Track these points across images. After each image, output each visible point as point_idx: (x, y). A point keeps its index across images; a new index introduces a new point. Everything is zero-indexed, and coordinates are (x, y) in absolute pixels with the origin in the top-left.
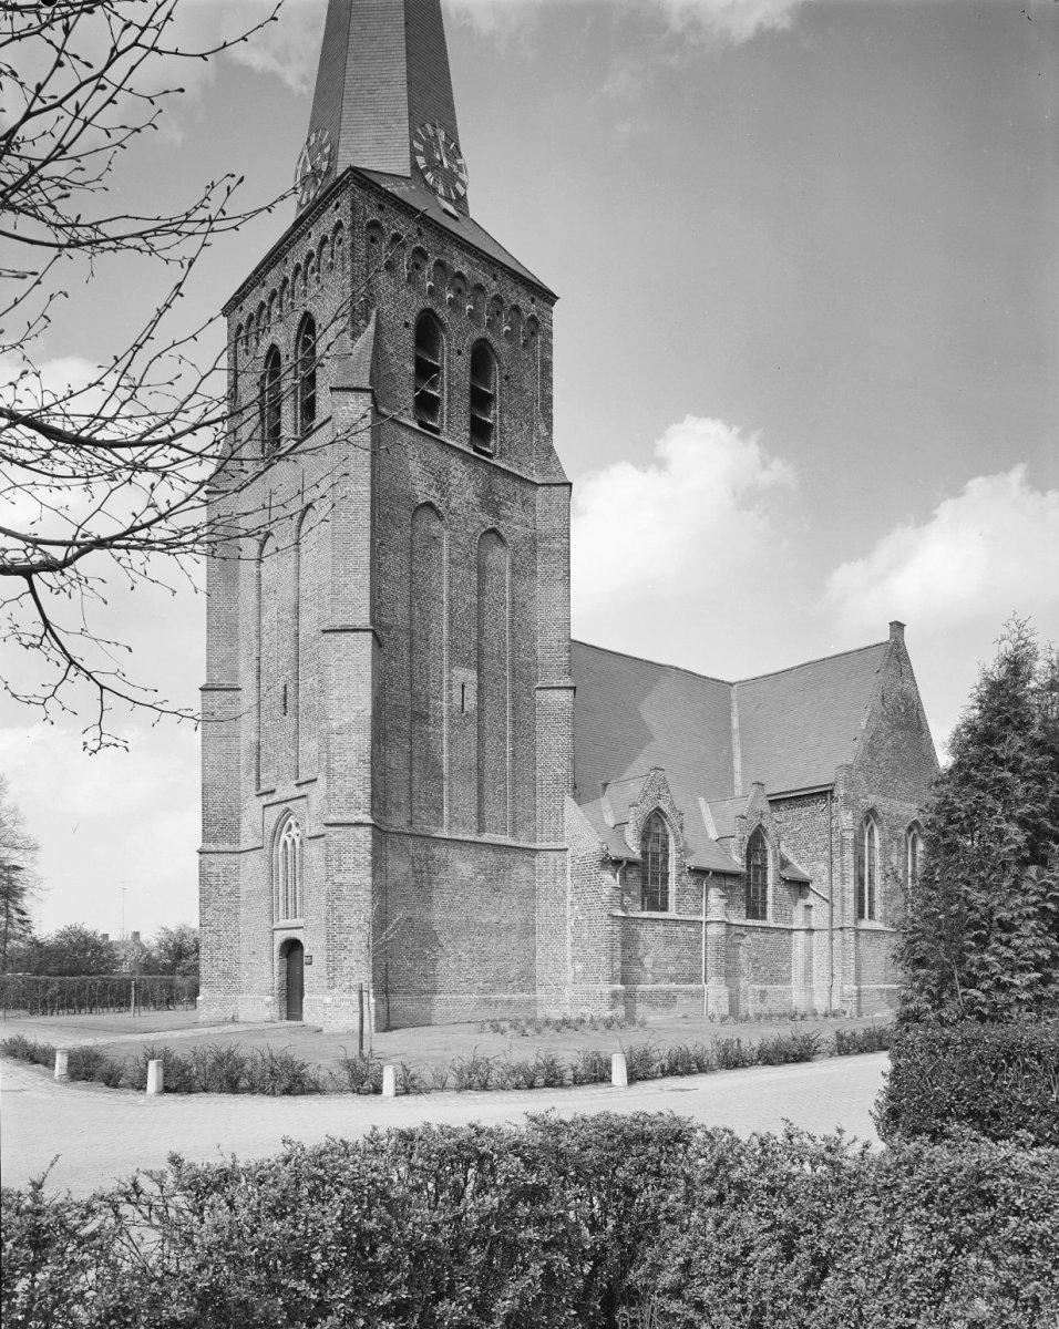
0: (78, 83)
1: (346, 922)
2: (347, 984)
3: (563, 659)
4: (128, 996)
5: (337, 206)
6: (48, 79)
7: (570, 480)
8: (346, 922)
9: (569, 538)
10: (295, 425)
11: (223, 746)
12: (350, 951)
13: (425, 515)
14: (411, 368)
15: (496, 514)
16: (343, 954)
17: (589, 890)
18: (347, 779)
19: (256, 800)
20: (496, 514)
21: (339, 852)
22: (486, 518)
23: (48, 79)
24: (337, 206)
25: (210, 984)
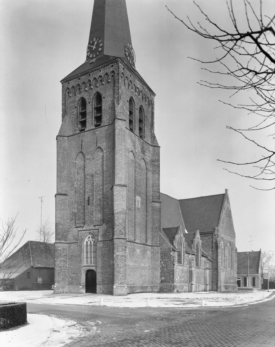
0: (262, 53)
1: (119, 266)
2: (120, 282)
3: (158, 195)
4: (267, 287)
5: (112, 66)
6: (228, 48)
7: (160, 146)
8: (119, 266)
9: (159, 162)
10: (135, 127)
11: (62, 212)
12: (120, 273)
13: (99, 149)
14: (128, 113)
15: (144, 154)
16: (119, 274)
17: (166, 258)
18: (119, 226)
19: (75, 229)
20: (144, 154)
21: (118, 246)
22: (142, 155)
23: (228, 48)
24: (112, 66)
25: (58, 282)
